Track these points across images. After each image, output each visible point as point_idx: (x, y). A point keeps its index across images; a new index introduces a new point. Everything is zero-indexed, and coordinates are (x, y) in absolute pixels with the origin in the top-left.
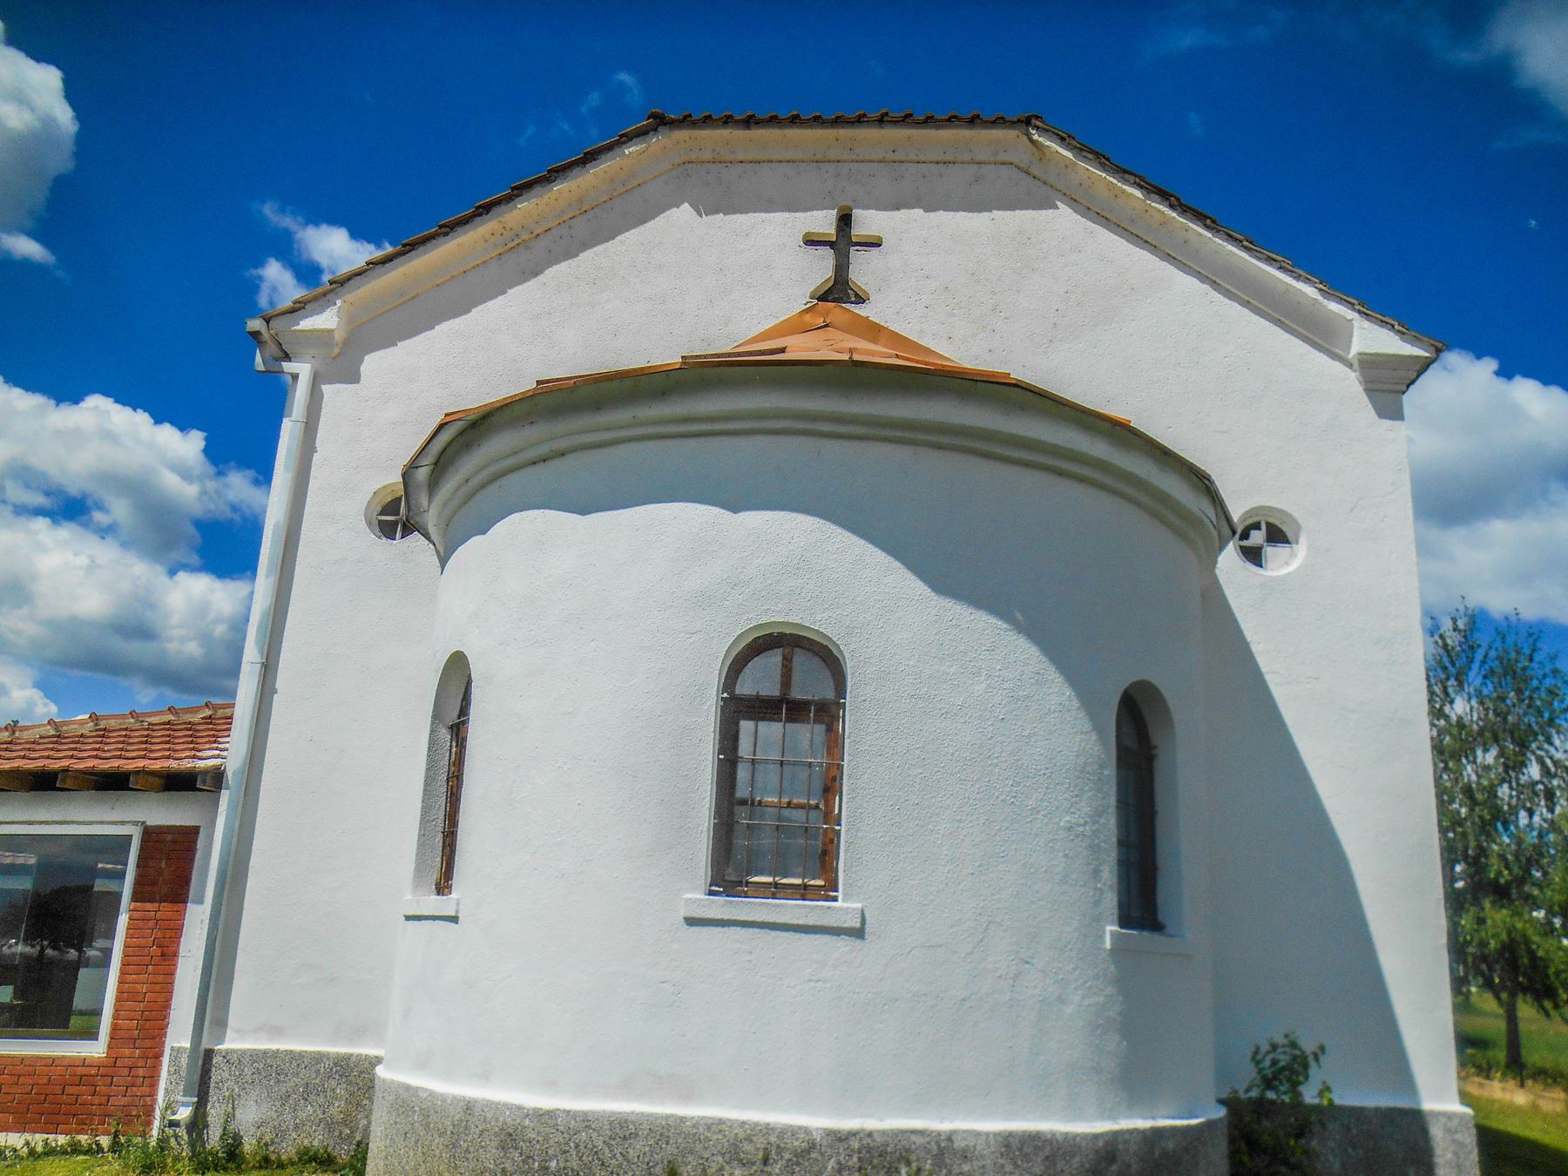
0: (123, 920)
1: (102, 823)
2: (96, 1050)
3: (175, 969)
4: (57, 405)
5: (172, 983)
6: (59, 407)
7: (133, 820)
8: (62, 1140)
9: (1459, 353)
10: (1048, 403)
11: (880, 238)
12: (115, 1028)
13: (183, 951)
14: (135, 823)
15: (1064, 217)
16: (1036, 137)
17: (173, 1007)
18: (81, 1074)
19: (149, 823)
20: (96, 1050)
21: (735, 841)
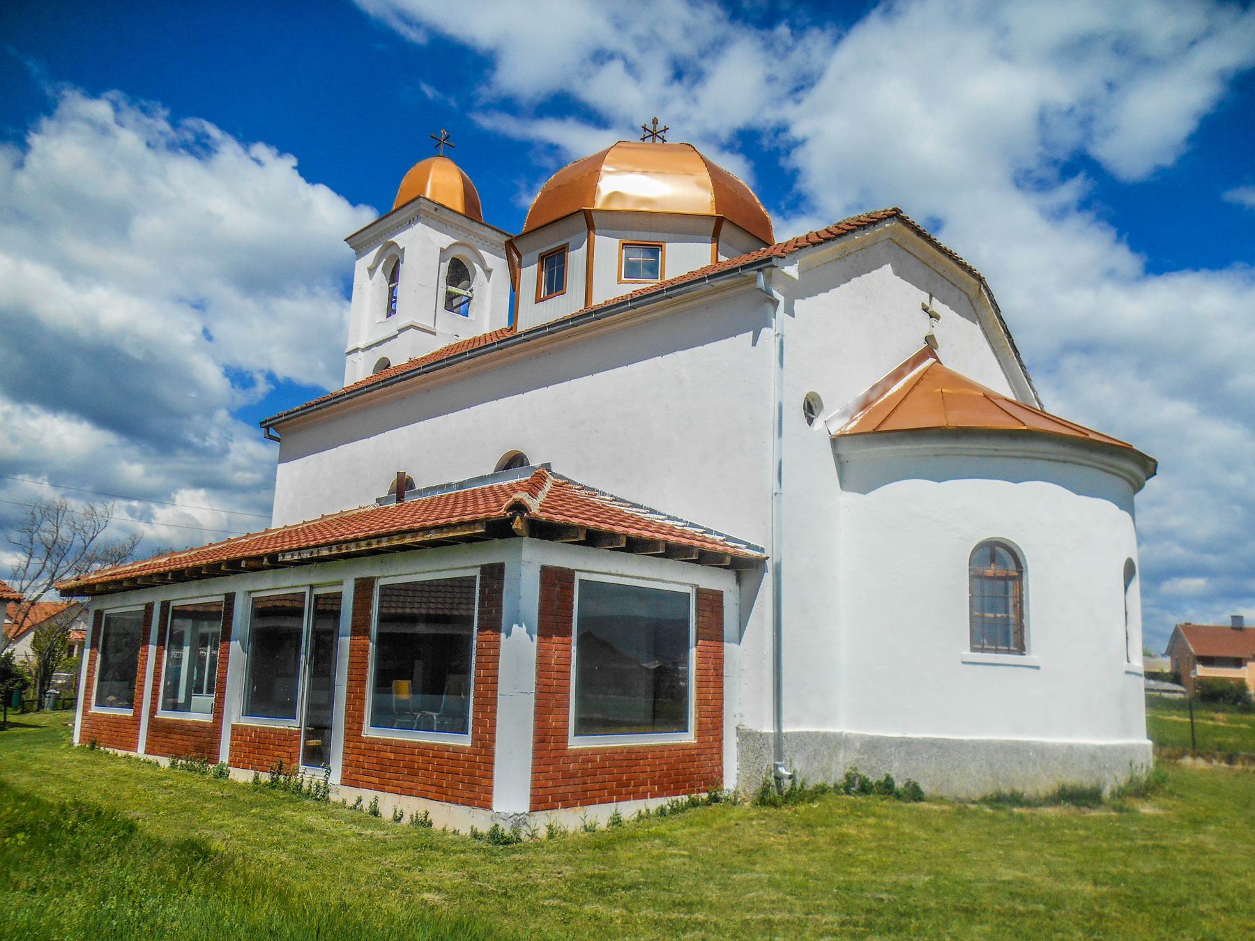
0: (693, 652)
1: (424, 572)
2: (688, 738)
3: (723, 684)
4: (294, 168)
5: (722, 693)
6: (293, 170)
7: (691, 583)
8: (684, 799)
9: (371, 209)
10: (365, 232)
11: (940, 317)
12: (700, 724)
13: (727, 673)
14: (692, 585)
15: (977, 328)
16: (982, 289)
17: (725, 708)
18: (687, 754)
19: (700, 587)
20: (688, 738)
21: (206, 622)
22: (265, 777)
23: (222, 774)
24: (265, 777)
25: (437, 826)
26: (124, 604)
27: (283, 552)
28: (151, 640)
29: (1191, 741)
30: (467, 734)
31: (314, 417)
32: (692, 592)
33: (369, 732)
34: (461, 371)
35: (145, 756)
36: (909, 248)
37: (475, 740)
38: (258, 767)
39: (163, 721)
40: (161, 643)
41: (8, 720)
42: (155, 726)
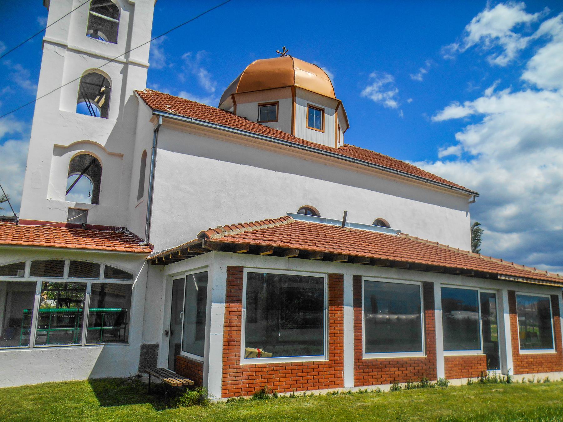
5: (355, 323)
22: (475, 380)
23: (443, 384)
24: (475, 380)
25: (551, 380)
26: (290, 268)
27: (501, 275)
28: (505, 310)
29: (43, 334)
30: (324, 355)
31: (220, 134)
32: (549, 297)
33: (366, 357)
34: (359, 168)
35: (357, 389)
36: (465, 193)
37: (329, 357)
38: (469, 376)
39: (368, 361)
40: (357, 303)
41: (398, 368)
42: (360, 365)
